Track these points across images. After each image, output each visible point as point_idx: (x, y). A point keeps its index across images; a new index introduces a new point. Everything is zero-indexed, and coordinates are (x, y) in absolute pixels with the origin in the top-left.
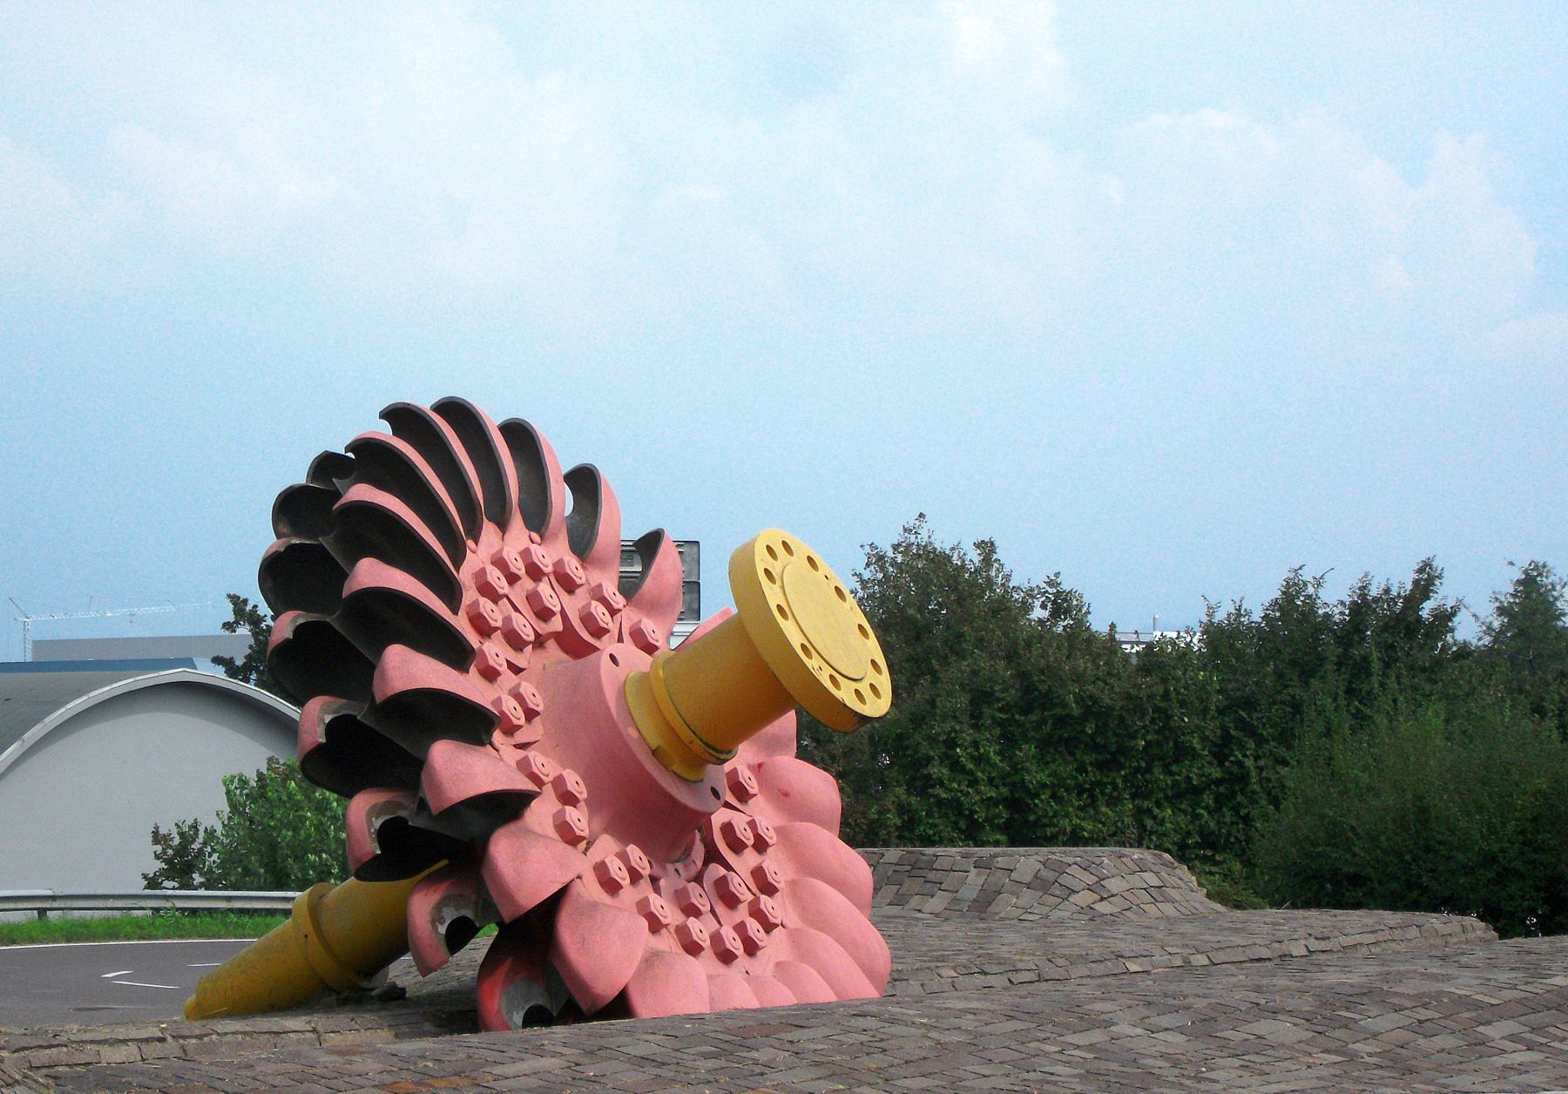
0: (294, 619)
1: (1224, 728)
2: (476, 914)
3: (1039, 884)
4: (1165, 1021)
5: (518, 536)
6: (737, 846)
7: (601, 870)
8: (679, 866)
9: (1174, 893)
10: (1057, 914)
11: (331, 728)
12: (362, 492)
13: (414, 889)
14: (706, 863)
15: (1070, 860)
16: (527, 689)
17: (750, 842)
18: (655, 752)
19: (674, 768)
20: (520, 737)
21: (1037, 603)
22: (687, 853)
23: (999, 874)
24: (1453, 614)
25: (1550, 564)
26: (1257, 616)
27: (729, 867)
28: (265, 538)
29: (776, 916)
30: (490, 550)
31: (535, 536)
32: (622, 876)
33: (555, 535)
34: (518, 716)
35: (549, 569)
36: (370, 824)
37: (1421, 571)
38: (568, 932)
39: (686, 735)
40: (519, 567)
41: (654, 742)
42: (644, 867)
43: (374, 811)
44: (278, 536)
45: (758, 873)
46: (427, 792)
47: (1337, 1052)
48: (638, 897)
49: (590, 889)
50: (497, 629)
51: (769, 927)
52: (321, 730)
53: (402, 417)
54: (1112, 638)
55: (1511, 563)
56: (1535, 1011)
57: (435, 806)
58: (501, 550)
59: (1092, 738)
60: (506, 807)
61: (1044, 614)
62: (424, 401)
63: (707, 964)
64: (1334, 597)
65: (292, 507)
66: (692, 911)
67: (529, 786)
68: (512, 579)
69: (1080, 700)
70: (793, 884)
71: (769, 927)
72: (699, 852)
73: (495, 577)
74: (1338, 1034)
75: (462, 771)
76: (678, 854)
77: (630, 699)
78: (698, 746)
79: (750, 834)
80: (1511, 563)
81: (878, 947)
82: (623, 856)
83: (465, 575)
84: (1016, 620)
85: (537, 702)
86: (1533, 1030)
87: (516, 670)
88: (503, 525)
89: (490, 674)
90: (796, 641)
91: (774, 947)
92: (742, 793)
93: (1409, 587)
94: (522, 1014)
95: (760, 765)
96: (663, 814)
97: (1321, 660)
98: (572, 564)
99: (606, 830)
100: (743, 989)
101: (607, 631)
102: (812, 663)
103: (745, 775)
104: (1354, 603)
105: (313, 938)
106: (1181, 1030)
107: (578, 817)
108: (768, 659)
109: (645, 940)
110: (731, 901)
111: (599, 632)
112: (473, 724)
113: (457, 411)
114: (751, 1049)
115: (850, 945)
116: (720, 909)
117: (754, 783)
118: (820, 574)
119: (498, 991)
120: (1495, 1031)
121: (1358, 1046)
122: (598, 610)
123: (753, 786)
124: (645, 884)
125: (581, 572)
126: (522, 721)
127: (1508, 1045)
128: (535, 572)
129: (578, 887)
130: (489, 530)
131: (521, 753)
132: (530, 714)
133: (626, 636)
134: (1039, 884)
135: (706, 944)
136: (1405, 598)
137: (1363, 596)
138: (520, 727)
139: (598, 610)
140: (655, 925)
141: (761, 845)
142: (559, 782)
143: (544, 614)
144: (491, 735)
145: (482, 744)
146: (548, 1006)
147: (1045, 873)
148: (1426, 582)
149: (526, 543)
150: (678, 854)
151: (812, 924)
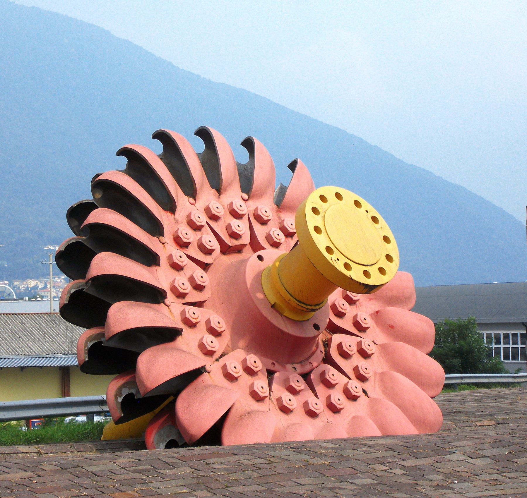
39: (287, 297)
41: (273, 299)
77: (263, 278)
81: (431, 409)
94: (165, 444)
95: (377, 312)
119: (154, 432)
145: (158, 303)
146: (177, 440)
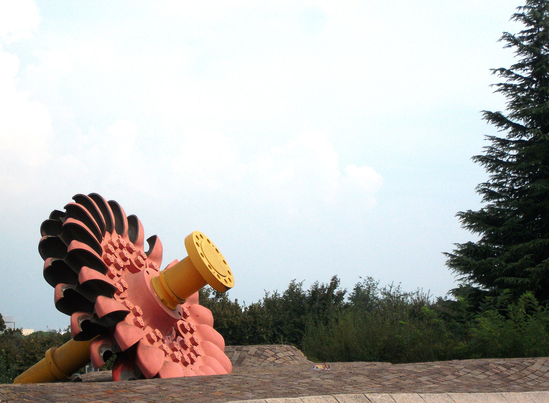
0: (51, 260)
1: (274, 332)
2: (112, 349)
3: (256, 355)
4: (326, 377)
5: (115, 237)
6: (185, 331)
7: (148, 336)
8: (169, 336)
9: (298, 358)
10: (263, 364)
11: (65, 293)
12: (71, 220)
13: (91, 343)
14: (177, 336)
15: (266, 348)
16: (123, 281)
17: (189, 330)
18: (162, 301)
19: (168, 305)
20: (122, 296)
21: (211, 293)
22: (171, 333)
23: (244, 352)
24: (344, 293)
25: (373, 277)
26: (281, 296)
27: (183, 338)
28: (38, 237)
29: (199, 352)
30: (109, 239)
31: (120, 236)
32: (155, 338)
33: (126, 236)
34: (121, 289)
35: (125, 246)
36: (79, 322)
37: (333, 280)
38: (141, 354)
39: (172, 295)
40: (117, 245)
41: (162, 297)
42: (161, 337)
43: (79, 318)
44: (42, 236)
45: (192, 340)
46: (97, 311)
47: (379, 384)
48: (159, 345)
49: (145, 342)
50: (112, 263)
51: (197, 355)
52: (62, 293)
53: (79, 198)
54: (236, 303)
55: (361, 277)
56: (432, 374)
57: (100, 315)
58: (111, 239)
59: (231, 336)
60: (120, 316)
61: (214, 296)
62: (86, 193)
63: (179, 365)
64: (306, 289)
65: (46, 227)
66: (174, 349)
67: (127, 310)
68: (115, 248)
69: (227, 323)
70: (202, 343)
71: (197, 355)
72: (174, 333)
73: (110, 247)
74: (378, 379)
75: (107, 305)
76: (168, 333)
78: (175, 299)
79: (189, 327)
80: (361, 277)
82: (155, 333)
83: (102, 245)
84: (205, 299)
85: (126, 285)
86: (433, 379)
87: (119, 276)
88: (111, 233)
89: (112, 276)
90: (207, 264)
91: (199, 361)
92: (185, 316)
93: (329, 285)
95: (190, 307)
96: (164, 320)
97: (303, 309)
98: (131, 245)
99: (148, 325)
100: (192, 372)
101: (143, 265)
102: (212, 271)
103: (186, 310)
104: (313, 291)
105: (53, 364)
106: (331, 379)
107: (140, 319)
108: (199, 270)
109: (164, 359)
110: (185, 347)
111: (141, 265)
112: (109, 291)
113: (95, 197)
114: (208, 383)
115: (221, 362)
116: (182, 350)
117: (188, 312)
118: (211, 245)
120: (423, 379)
121: (385, 383)
122: (140, 259)
123: (188, 313)
124: (160, 341)
125: (134, 247)
126: (122, 291)
127: (427, 383)
128: (121, 247)
129: (142, 341)
130: (107, 233)
131: (122, 301)
132: (125, 289)
133: (148, 266)
134: (256, 355)
135: (180, 360)
136: (328, 289)
137: (316, 289)
138: (122, 292)
139: (140, 259)
140: (166, 354)
141: (192, 331)
142: (134, 309)
143: (125, 259)
144: (113, 295)
147: (258, 352)
148: (335, 283)
149: (118, 238)
150: (168, 333)
151: (208, 354)
